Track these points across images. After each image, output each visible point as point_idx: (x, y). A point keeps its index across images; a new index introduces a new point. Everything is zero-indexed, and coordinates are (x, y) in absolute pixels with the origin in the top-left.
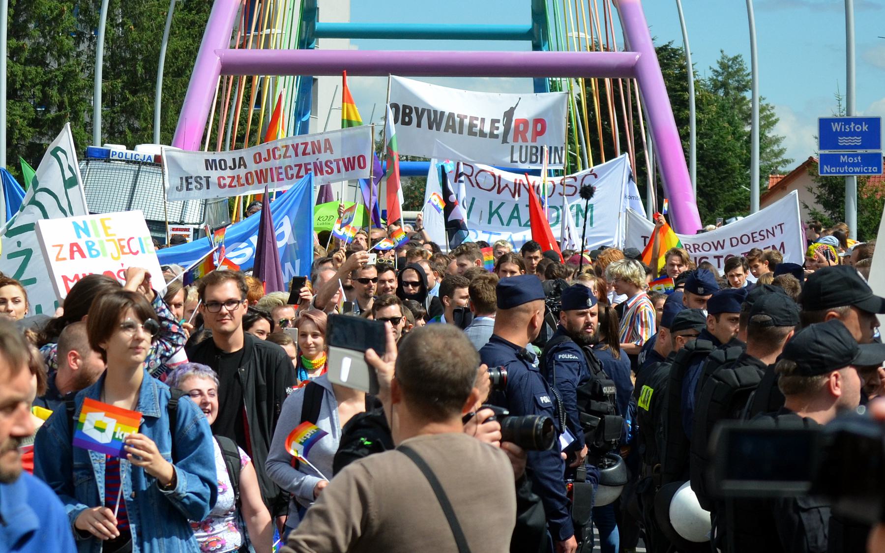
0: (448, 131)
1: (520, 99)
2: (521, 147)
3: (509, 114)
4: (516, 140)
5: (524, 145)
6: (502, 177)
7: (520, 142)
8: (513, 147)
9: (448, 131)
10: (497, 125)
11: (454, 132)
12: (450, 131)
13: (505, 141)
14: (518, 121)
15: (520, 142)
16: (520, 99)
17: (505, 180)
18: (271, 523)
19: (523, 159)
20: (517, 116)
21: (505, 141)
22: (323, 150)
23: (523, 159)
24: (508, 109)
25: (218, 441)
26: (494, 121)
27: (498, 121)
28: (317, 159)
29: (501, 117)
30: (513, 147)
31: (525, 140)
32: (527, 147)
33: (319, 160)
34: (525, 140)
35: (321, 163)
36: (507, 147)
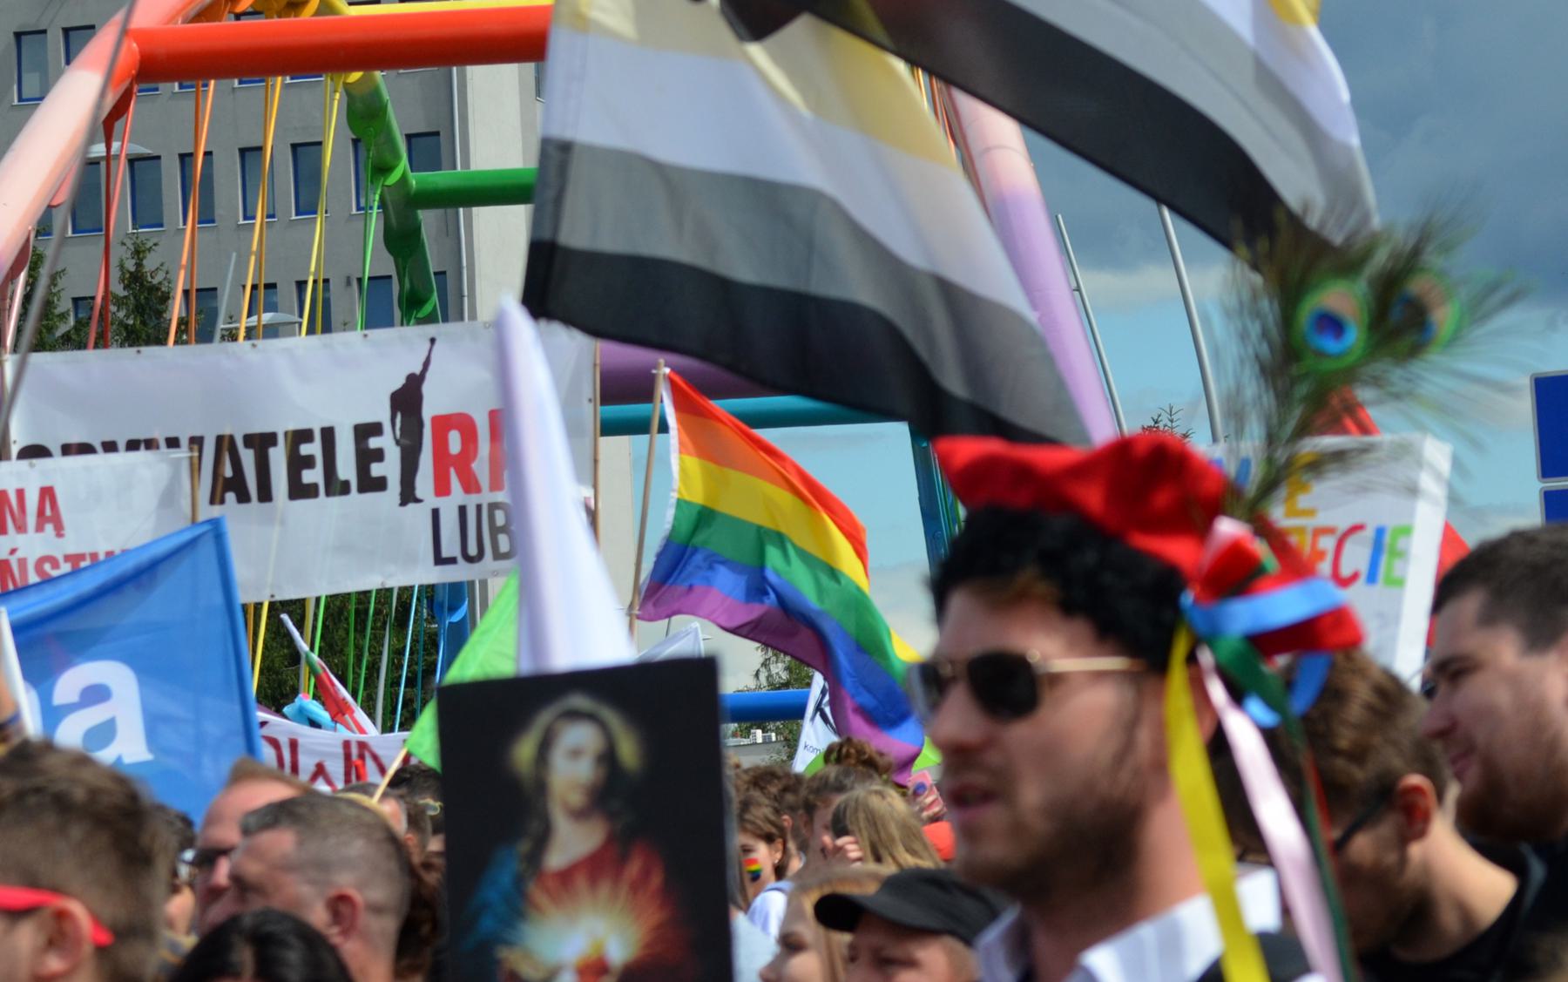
0: (222, 502)
1: (433, 341)
2: (462, 510)
3: (407, 399)
4: (442, 489)
5: (471, 501)
6: (301, 741)
7: (457, 495)
8: (436, 513)
9: (222, 502)
10: (374, 443)
11: (243, 497)
12: (230, 497)
13: (408, 495)
14: (444, 424)
15: (457, 495)
16: (433, 341)
17: (312, 753)
18: (830, 562)
19: (473, 550)
20: (433, 404)
21: (408, 495)
22: (31, 519)
23: (473, 550)
24: (398, 382)
25: (681, 459)
26: (364, 432)
27: (375, 429)
28: (13, 551)
29: (380, 412)
30: (436, 513)
31: (470, 485)
32: (479, 508)
33: (19, 554)
34: (470, 485)
35: (23, 563)
36: (417, 516)
